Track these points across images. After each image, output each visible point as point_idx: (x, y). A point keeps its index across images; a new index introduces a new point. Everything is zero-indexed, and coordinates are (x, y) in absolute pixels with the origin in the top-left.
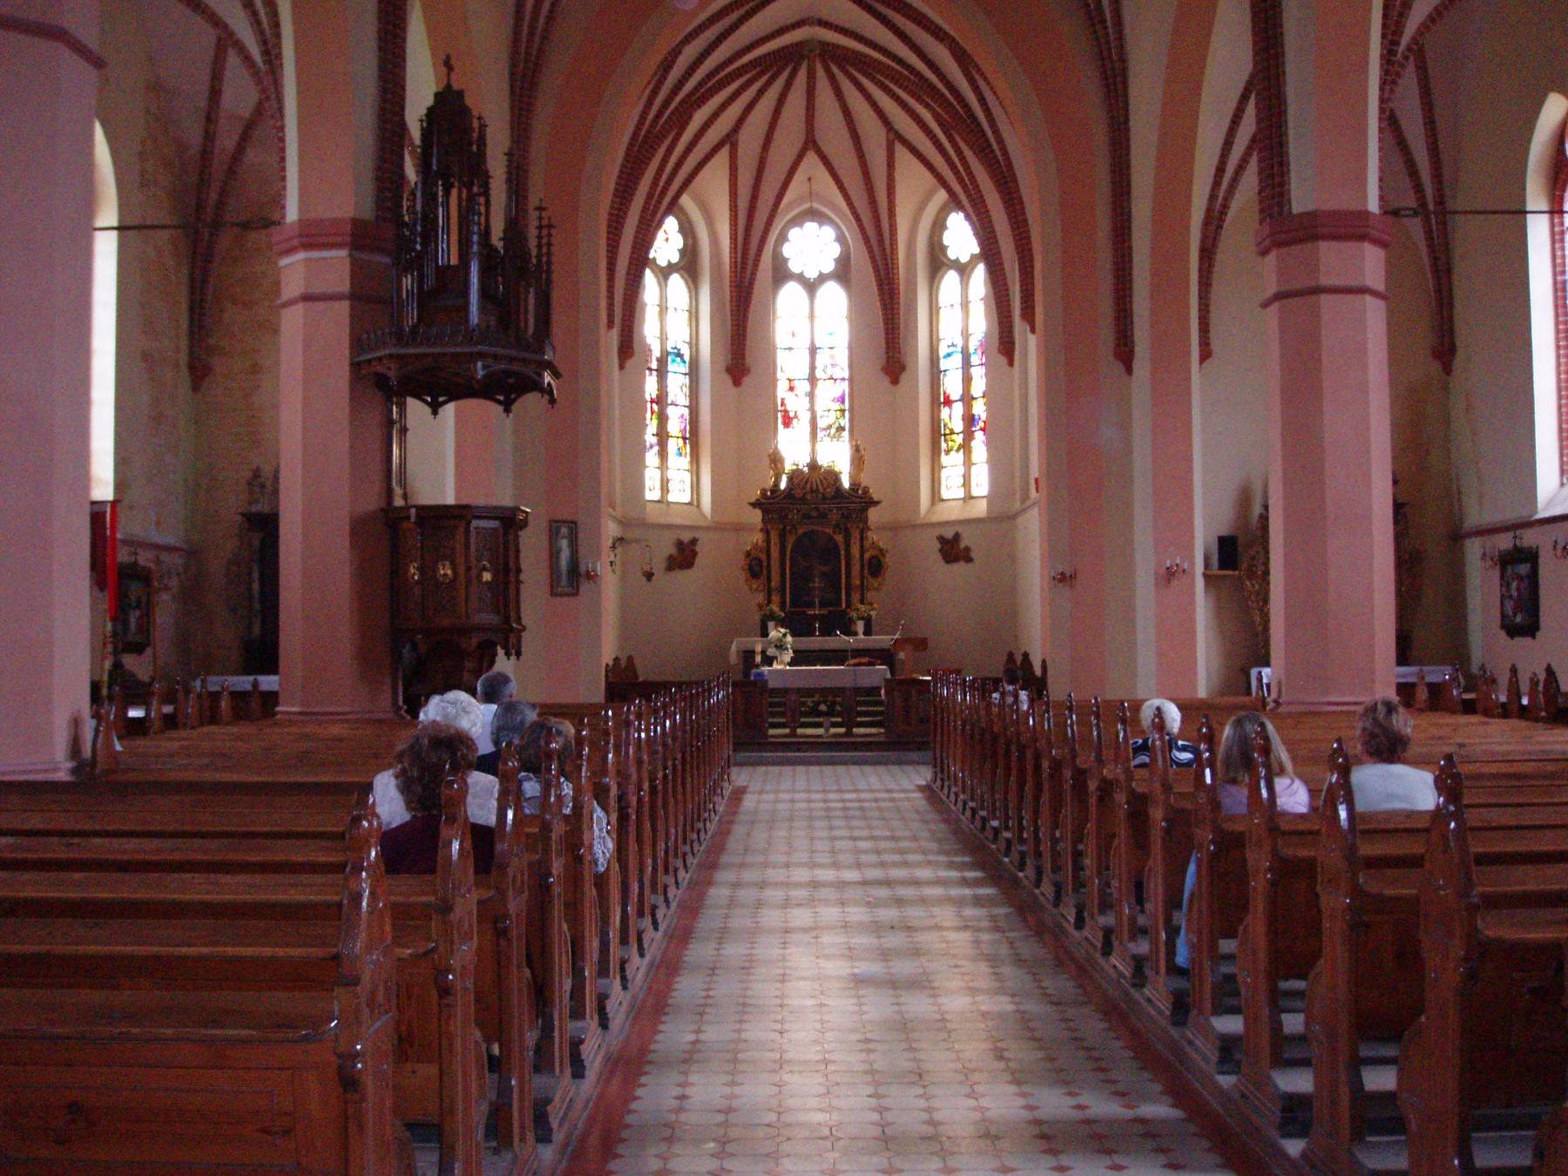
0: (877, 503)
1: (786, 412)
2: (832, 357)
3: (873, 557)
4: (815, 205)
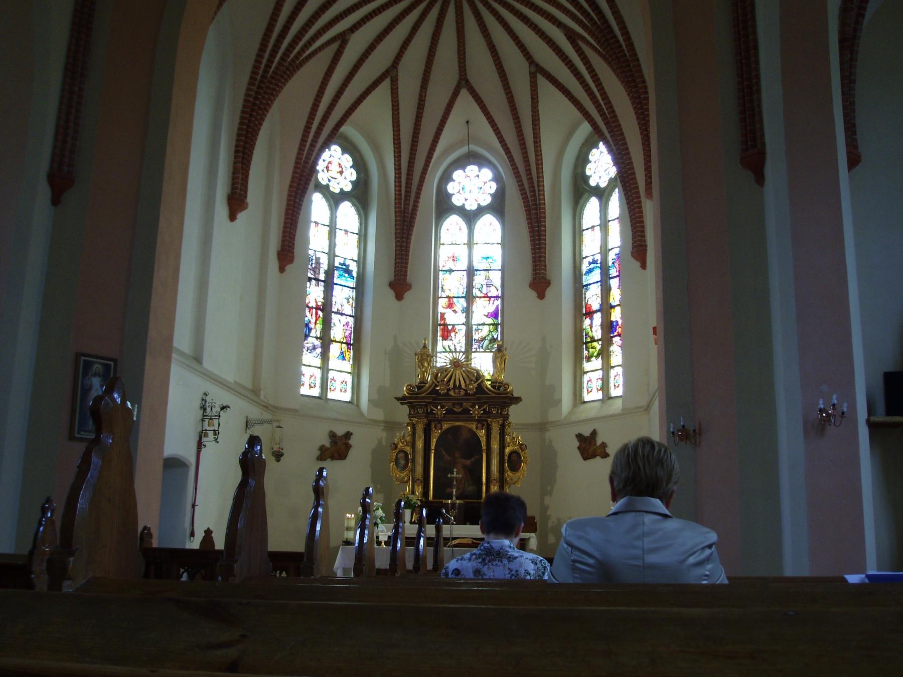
0: (518, 400)
1: (445, 325)
2: (488, 278)
3: (511, 453)
4: (474, 148)
